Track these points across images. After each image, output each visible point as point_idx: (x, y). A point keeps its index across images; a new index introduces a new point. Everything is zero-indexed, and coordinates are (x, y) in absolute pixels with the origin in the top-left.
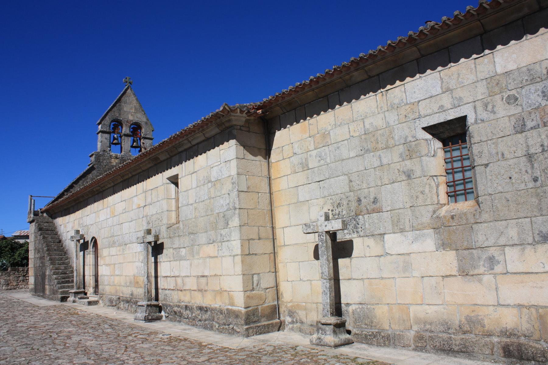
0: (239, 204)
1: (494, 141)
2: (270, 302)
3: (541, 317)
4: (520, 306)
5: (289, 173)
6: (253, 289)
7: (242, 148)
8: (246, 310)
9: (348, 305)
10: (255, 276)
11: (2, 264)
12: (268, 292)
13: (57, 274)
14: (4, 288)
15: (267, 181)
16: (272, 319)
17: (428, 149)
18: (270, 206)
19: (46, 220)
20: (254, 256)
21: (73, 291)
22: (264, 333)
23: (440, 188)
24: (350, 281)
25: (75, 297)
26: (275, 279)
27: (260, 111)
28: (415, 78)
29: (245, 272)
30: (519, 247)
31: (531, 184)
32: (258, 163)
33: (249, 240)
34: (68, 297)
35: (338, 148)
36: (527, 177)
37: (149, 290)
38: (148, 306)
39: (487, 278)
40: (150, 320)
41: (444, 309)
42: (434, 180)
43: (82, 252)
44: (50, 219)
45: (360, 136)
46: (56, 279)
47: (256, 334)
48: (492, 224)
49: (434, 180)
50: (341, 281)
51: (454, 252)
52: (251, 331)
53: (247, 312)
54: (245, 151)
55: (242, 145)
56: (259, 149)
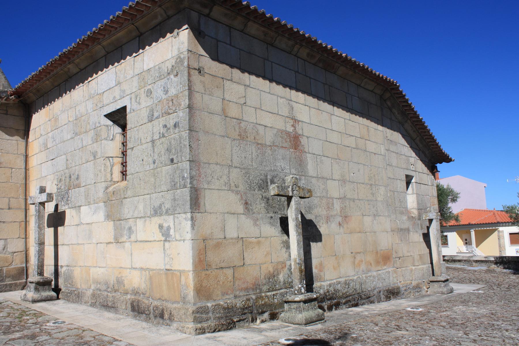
1: (138, 128)
2: (18, 263)
3: (151, 278)
4: (142, 269)
5: (38, 152)
9: (62, 266)
12: (16, 256)
15: (23, 158)
16: (18, 280)
17: (108, 133)
22: (5, 291)
23: (114, 168)
26: (24, 244)
27: (13, 97)
28: (103, 72)
30: (143, 219)
31: (152, 166)
32: (14, 142)
35: (62, 131)
36: (151, 160)
39: (127, 245)
41: (107, 271)
42: (110, 161)
43: (52, 229)
45: (73, 121)
48: (131, 199)
49: (110, 161)
50: (59, 246)
51: (112, 222)
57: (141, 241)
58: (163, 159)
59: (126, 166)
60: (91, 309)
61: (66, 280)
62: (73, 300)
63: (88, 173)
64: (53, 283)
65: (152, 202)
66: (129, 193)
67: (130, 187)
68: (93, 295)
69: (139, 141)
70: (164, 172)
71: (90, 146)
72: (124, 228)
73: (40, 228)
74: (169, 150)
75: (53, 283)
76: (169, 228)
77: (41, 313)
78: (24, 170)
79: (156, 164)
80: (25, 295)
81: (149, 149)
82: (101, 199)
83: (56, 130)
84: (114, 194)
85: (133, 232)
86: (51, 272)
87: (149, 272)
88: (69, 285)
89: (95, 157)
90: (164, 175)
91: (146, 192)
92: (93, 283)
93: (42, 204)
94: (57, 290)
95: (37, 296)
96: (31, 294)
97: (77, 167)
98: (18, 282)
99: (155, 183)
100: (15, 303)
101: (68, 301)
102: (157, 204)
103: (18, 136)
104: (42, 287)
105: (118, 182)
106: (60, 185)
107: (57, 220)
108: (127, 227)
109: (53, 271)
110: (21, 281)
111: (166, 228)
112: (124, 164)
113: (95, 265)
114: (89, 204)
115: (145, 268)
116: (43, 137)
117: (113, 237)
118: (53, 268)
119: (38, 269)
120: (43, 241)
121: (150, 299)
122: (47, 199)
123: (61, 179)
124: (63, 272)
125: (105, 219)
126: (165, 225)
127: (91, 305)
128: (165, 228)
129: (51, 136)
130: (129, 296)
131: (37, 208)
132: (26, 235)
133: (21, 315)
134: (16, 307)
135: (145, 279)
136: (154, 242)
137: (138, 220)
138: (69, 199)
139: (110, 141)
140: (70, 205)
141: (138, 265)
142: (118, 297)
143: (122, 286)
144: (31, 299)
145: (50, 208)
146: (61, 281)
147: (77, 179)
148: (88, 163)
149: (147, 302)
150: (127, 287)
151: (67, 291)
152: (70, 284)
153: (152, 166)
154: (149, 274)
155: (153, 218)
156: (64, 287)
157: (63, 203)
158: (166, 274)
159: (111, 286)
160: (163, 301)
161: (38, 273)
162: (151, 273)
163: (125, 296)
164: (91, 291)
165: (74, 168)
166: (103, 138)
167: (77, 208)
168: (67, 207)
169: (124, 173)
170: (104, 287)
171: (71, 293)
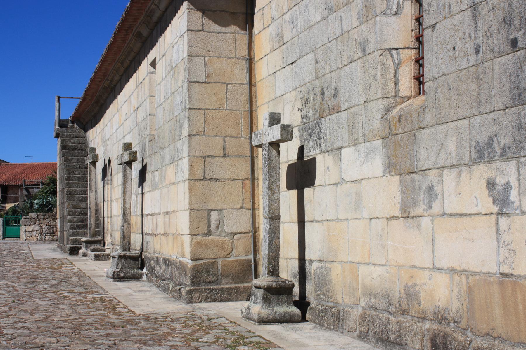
0: (190, 101)
2: (241, 253)
3: (470, 290)
4: (452, 271)
6: (209, 233)
7: (200, 14)
8: (194, 263)
9: (311, 261)
10: (212, 213)
11: (47, 202)
12: (238, 240)
13: (74, 214)
14: (47, 238)
15: (244, 65)
16: (243, 282)
18: (248, 106)
19: (75, 134)
20: (213, 182)
21: (84, 239)
22: (221, 301)
24: (313, 223)
25: (87, 248)
29: (195, 207)
30: (456, 170)
32: (229, 36)
33: (204, 158)
34: (80, 248)
35: (307, 7)
36: (470, 47)
37: (126, 235)
38: (120, 257)
39: (425, 221)
40: (123, 278)
42: (392, 57)
43: (294, 193)
44: (83, 132)
46: (70, 221)
47: (206, 300)
48: (433, 130)
49: (392, 57)
50: (306, 224)
51: (398, 177)
52: (196, 295)
53: (194, 267)
54: (205, 20)
55: (198, 9)
56: (234, 14)
57: (451, 215)
58: (495, 42)
59: (421, 65)
60: (358, 343)
61: (318, 287)
62: (329, 324)
63: (355, 84)
64: (296, 290)
65: (473, 133)
66: (429, 118)
67: (431, 105)
68: (364, 318)
69: (447, 10)
70: (497, 70)
71: (356, 30)
72: (420, 188)
73: (273, 189)
74: (507, 22)
75: (296, 290)
76: (507, 187)
77: (270, 342)
78: (247, 87)
79: (481, 54)
80: (248, 308)
81: (467, 24)
82: (376, 132)
83: (297, 7)
84: (399, 121)
85: (436, 195)
86: (294, 271)
87: (467, 278)
88: (322, 297)
89: (364, 51)
90: (496, 76)
91: (462, 113)
92: (364, 295)
93: (275, 145)
94: (303, 304)
95: (266, 312)
96: (257, 308)
97: (333, 74)
98: (242, 285)
99: (479, 94)
100: (231, 322)
101: (321, 325)
102: (483, 138)
103: (236, 25)
104: (275, 296)
105: (409, 98)
106: (307, 109)
107: (303, 175)
108: (424, 186)
109: (297, 269)
110: (246, 285)
111: (501, 187)
112: (419, 62)
113: (367, 261)
114: (356, 143)
115: (459, 269)
116: (275, 23)
117: (399, 206)
118: (296, 264)
119: (269, 263)
120: (276, 213)
121: (469, 334)
122: (281, 135)
123: (307, 100)
124: (312, 272)
125: (384, 172)
126: (500, 181)
127: (359, 337)
128: (499, 188)
129: (288, 20)
130: (427, 325)
131: (266, 153)
132: (254, 203)
133: (236, 342)
134: (231, 329)
135: (459, 292)
136: (477, 218)
137: (446, 171)
138: (322, 135)
139: (393, 18)
140: (323, 147)
141: (445, 264)
142: (407, 324)
143: (415, 303)
144: (256, 317)
145: (289, 153)
146: (310, 288)
147: (335, 96)
148: (353, 64)
149: (461, 338)
150: (424, 305)
151: (319, 307)
152: (324, 294)
153: (473, 59)
154: (467, 282)
155: (474, 168)
156: (315, 299)
157: (311, 144)
158: (501, 283)
159: (395, 302)
160: (495, 338)
161: (269, 272)
162: (470, 279)
163: (420, 325)
164: (360, 309)
165: (328, 76)
166: (378, 11)
167: (336, 152)
168: (318, 151)
169: (419, 80)
170: (382, 305)
171: (326, 310)
